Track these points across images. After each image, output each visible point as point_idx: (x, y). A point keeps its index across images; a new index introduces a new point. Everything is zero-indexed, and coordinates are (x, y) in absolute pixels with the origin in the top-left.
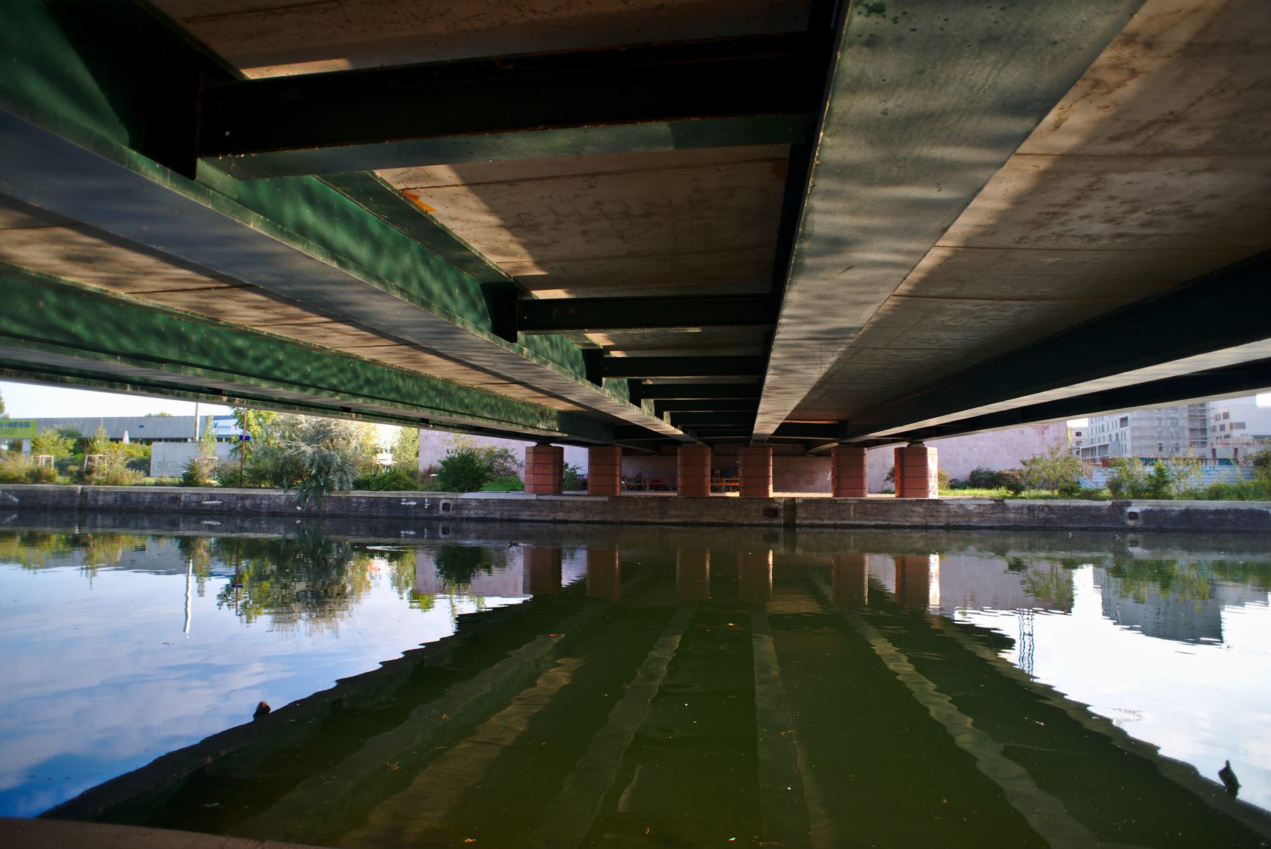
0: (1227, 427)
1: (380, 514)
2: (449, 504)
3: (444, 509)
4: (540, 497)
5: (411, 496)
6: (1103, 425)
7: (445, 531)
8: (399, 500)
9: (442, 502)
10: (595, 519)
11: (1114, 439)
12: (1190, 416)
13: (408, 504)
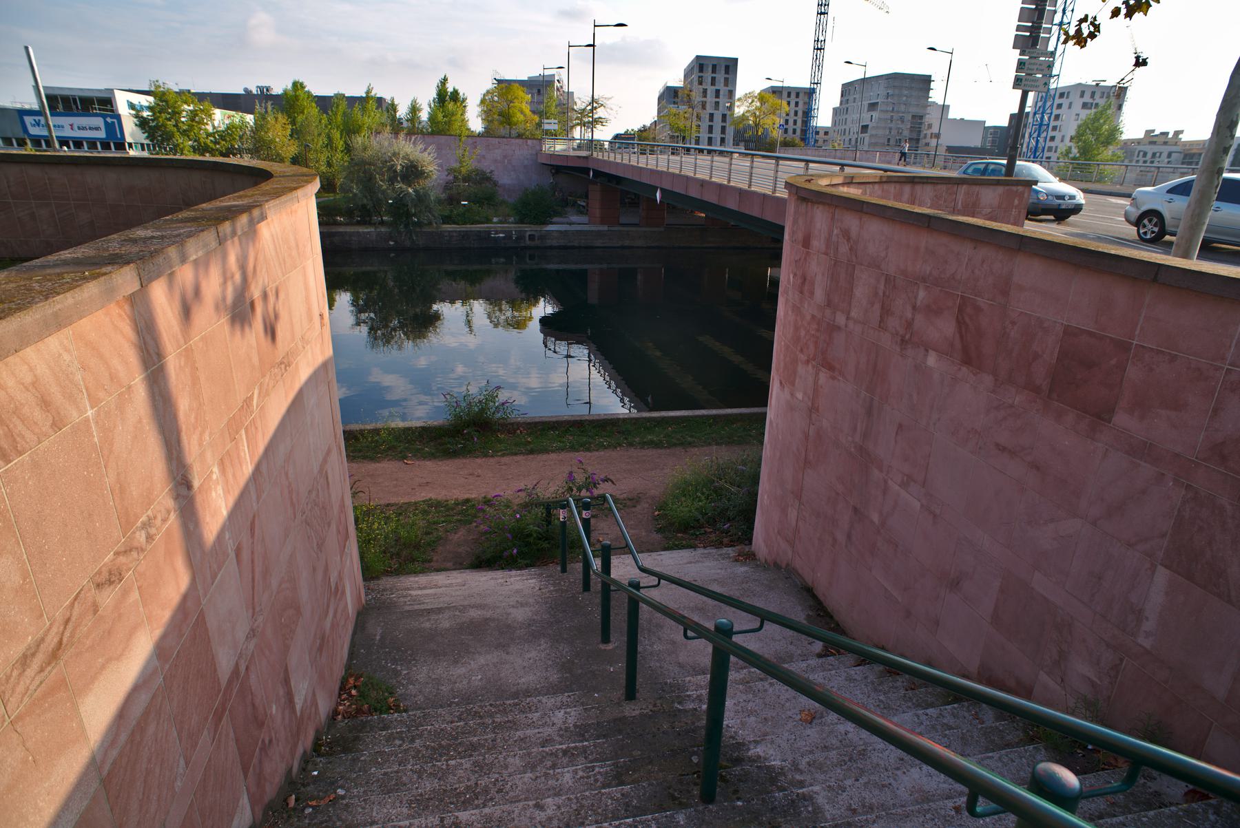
0: (929, 136)
1: (472, 246)
2: (533, 235)
3: (529, 239)
4: (610, 228)
5: (499, 229)
6: (845, 129)
7: (532, 257)
8: (489, 233)
9: (528, 234)
10: (653, 245)
11: (853, 142)
12: (911, 127)
13: (497, 236)
